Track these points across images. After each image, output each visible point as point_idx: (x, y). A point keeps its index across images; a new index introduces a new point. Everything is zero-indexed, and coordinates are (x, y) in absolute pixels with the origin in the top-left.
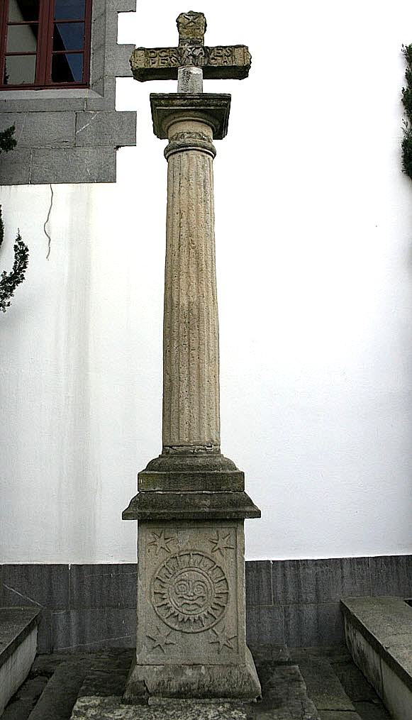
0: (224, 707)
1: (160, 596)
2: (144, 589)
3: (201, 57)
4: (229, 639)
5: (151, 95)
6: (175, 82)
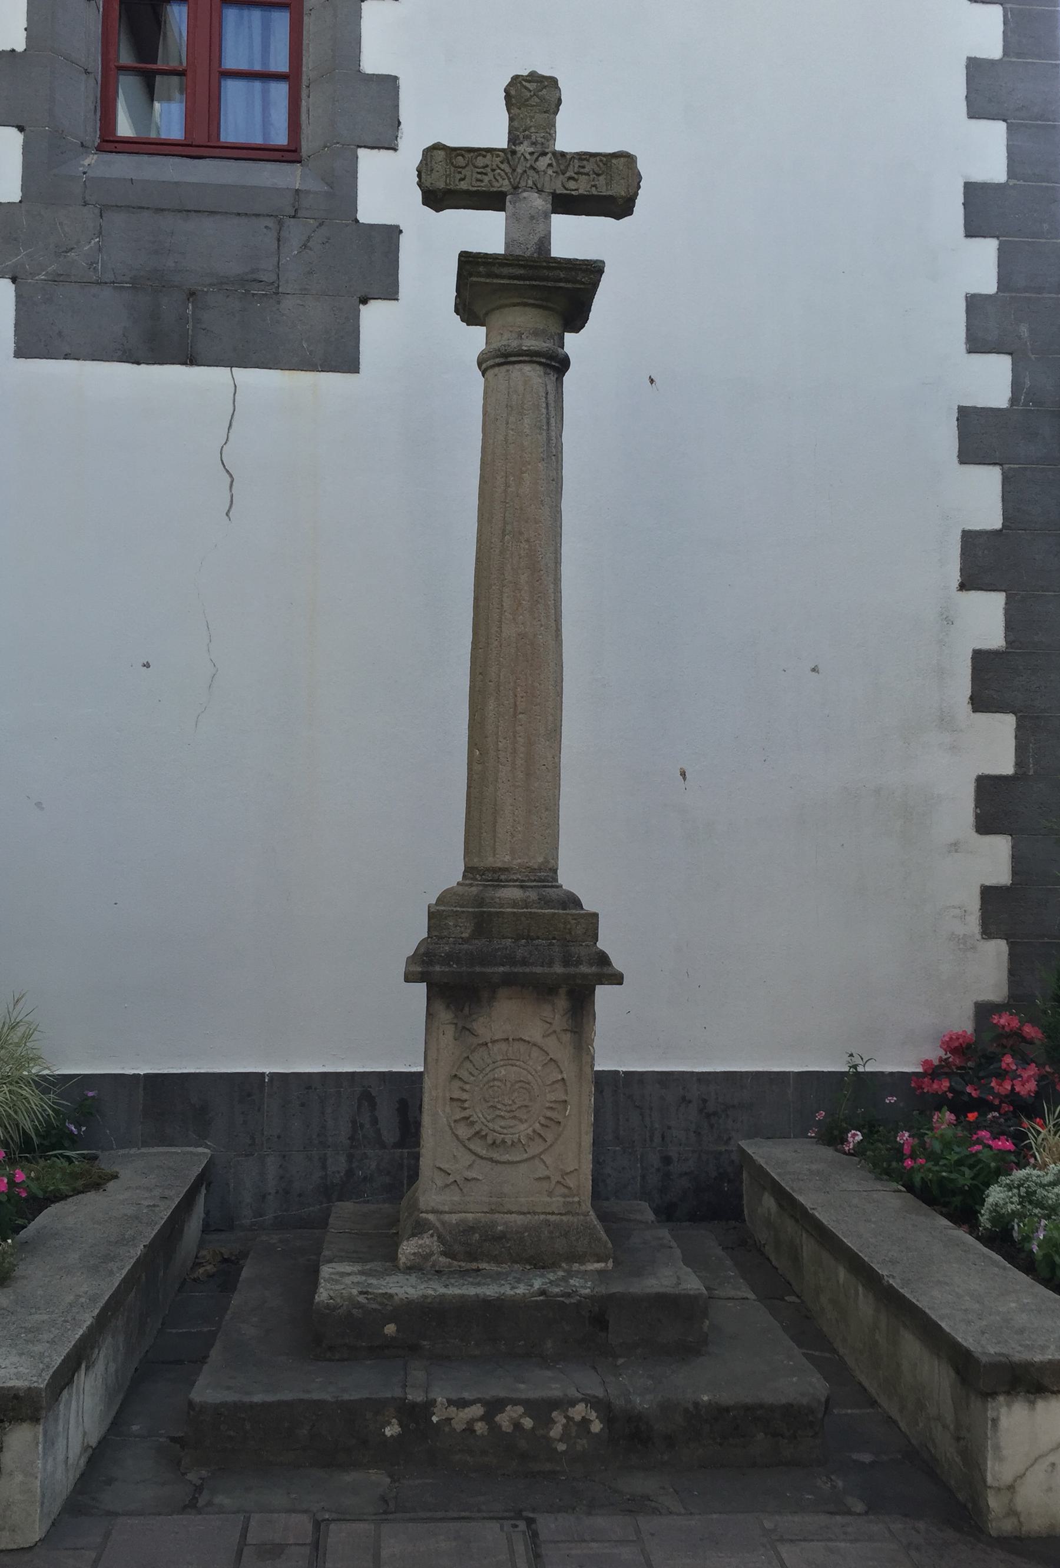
1: (459, 1104)
2: (434, 1094)
3: (550, 172)
6: (502, 215)
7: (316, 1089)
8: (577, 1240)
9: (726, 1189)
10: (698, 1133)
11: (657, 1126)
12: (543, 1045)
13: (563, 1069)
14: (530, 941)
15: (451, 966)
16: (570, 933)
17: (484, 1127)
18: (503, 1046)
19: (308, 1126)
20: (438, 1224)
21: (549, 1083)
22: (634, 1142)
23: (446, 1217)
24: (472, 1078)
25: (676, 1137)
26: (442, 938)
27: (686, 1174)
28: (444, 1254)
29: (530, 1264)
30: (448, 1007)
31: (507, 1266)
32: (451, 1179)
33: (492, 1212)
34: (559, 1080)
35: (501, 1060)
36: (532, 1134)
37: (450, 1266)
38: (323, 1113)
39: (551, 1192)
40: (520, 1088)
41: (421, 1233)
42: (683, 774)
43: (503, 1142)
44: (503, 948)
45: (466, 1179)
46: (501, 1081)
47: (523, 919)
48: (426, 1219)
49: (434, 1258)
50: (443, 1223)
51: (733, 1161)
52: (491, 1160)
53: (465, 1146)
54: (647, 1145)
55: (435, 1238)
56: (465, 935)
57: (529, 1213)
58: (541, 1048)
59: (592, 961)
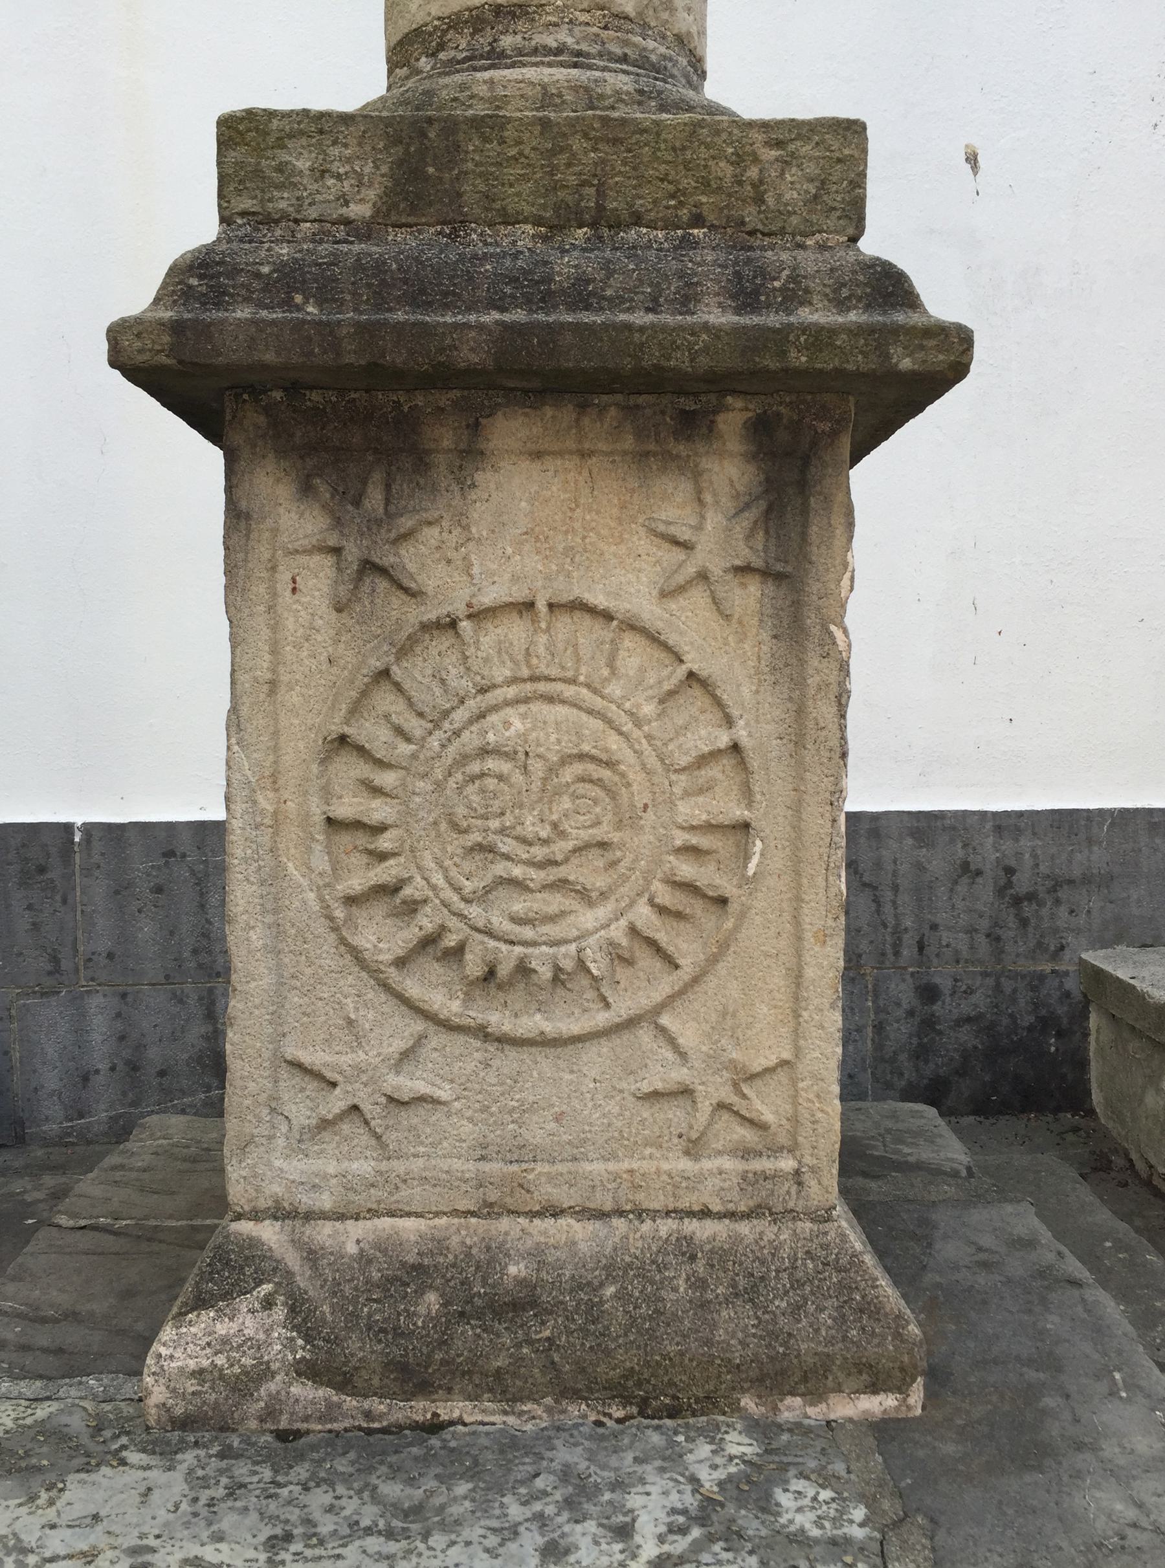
0: (51, 1095)
1: (362, 839)
4: (752, 1077)
5: (853, 130)
7: (184, 856)
8: (796, 1310)
9: (1053, 1049)
10: (994, 939)
11: (909, 923)
12: (660, 625)
13: (735, 712)
14: (605, 232)
15: (288, 304)
16: (759, 200)
17: (453, 922)
18: (515, 630)
19: (172, 933)
20: (293, 1260)
21: (684, 761)
22: (860, 956)
23: (323, 1233)
24: (405, 749)
25: (948, 946)
26: (270, 221)
27: (969, 1020)
28: (308, 1371)
29: (626, 1401)
30: (306, 489)
31: (539, 1411)
32: (336, 1103)
33: (489, 1210)
34: (720, 751)
35: (514, 680)
36: (624, 942)
37: (331, 1412)
38: (202, 906)
39: (695, 1142)
40: (582, 779)
41: (227, 1296)
42: (972, 159)
43: (523, 970)
44: (504, 254)
45: (391, 1099)
46: (510, 756)
47: (577, 143)
48: (253, 1243)
49: (272, 1386)
50: (312, 1256)
51: (1068, 995)
52: (482, 1033)
53: (386, 987)
54: (888, 964)
55: (279, 1313)
56: (359, 210)
57: (621, 1213)
58: (654, 638)
59: (845, 292)
